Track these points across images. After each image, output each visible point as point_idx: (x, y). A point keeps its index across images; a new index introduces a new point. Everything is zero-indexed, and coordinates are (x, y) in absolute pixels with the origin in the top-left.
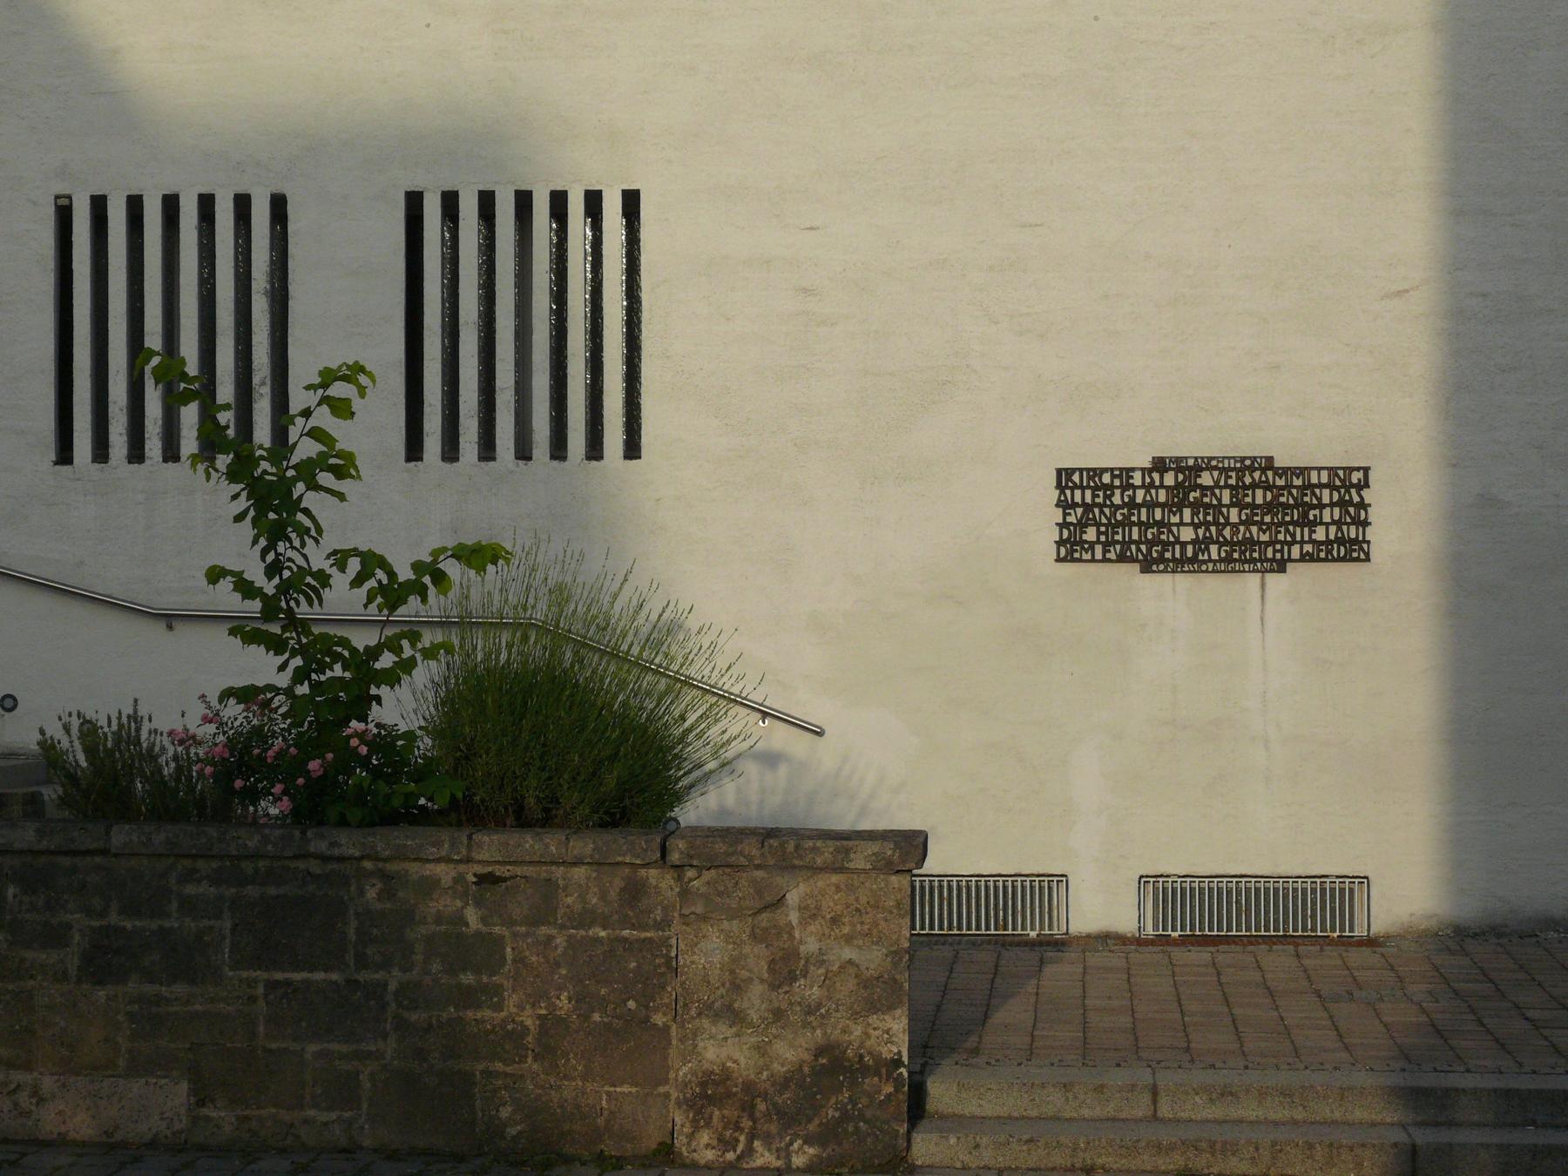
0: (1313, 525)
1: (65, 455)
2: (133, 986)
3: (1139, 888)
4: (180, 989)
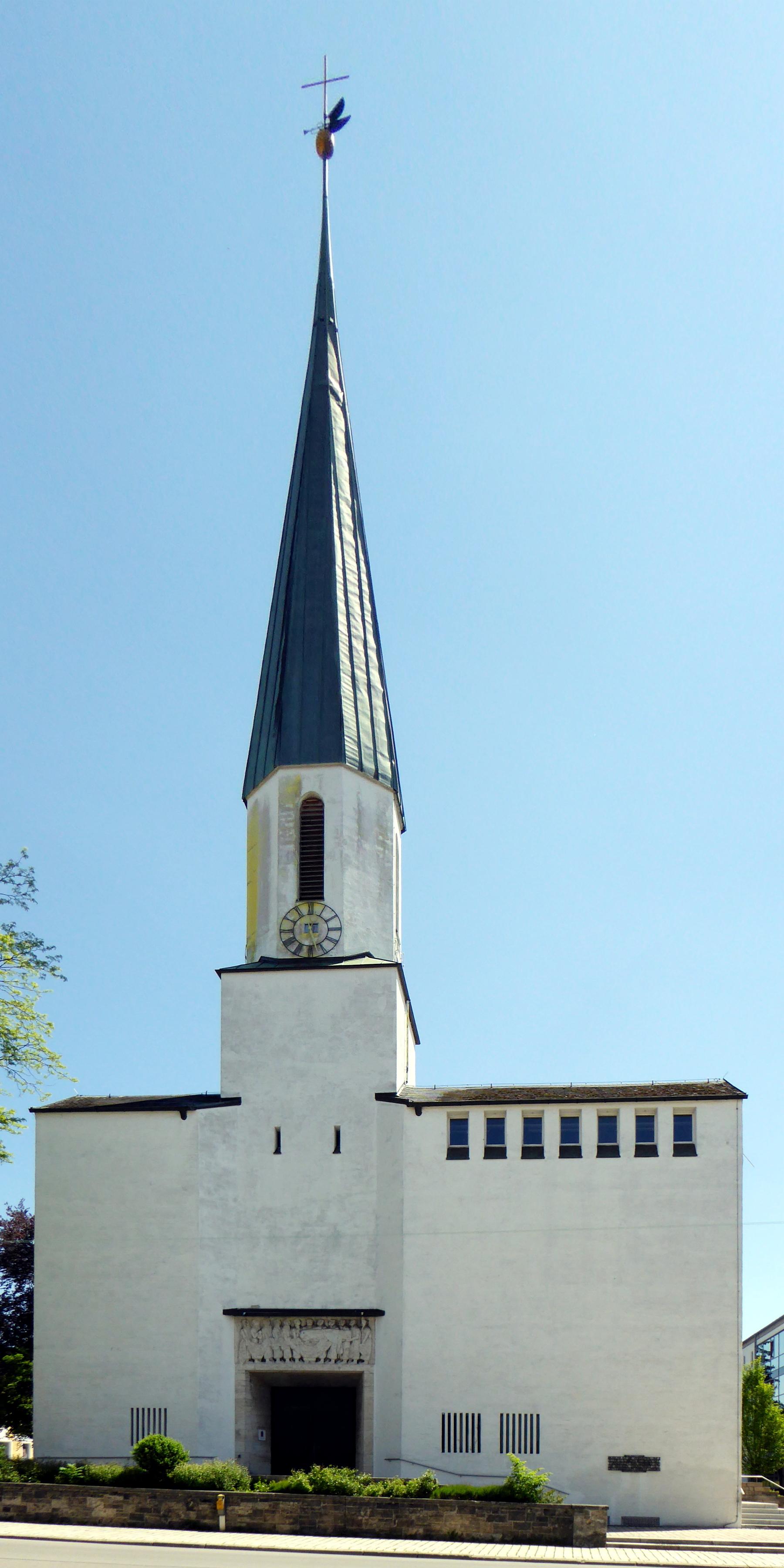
0: (650, 1465)
1: (443, 1451)
2: (494, 1522)
3: (281, 641)
4: (501, 1523)
